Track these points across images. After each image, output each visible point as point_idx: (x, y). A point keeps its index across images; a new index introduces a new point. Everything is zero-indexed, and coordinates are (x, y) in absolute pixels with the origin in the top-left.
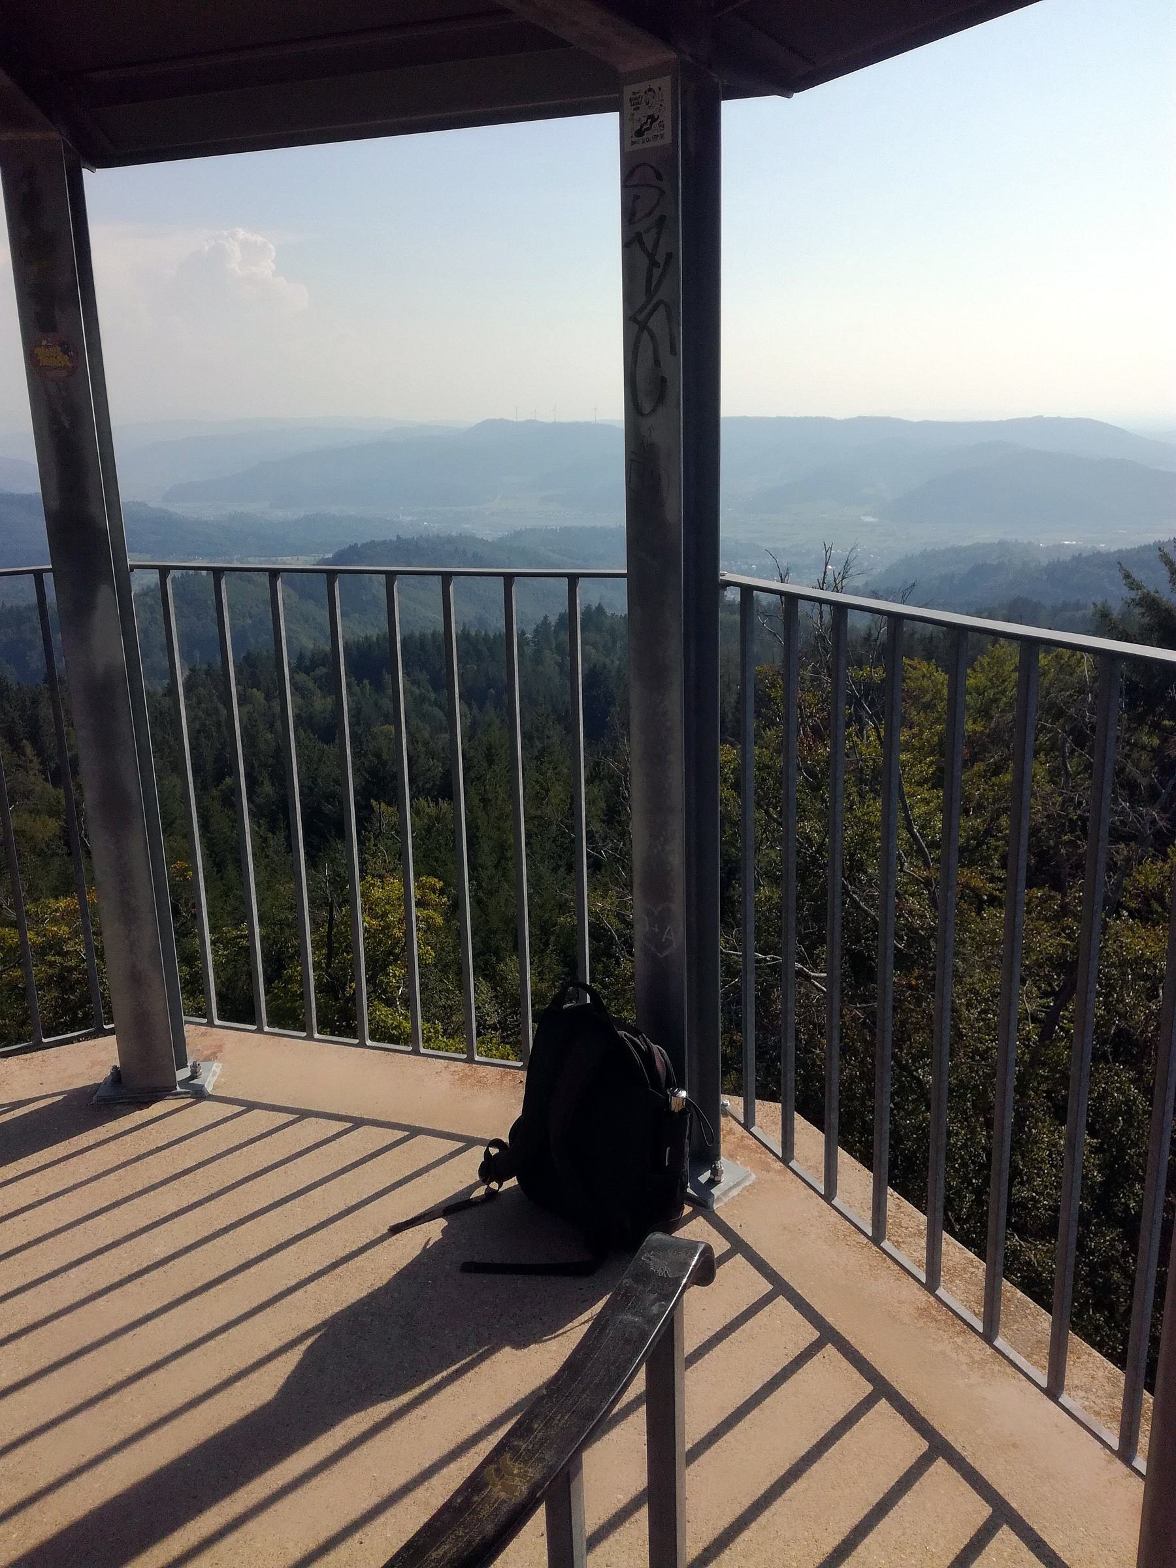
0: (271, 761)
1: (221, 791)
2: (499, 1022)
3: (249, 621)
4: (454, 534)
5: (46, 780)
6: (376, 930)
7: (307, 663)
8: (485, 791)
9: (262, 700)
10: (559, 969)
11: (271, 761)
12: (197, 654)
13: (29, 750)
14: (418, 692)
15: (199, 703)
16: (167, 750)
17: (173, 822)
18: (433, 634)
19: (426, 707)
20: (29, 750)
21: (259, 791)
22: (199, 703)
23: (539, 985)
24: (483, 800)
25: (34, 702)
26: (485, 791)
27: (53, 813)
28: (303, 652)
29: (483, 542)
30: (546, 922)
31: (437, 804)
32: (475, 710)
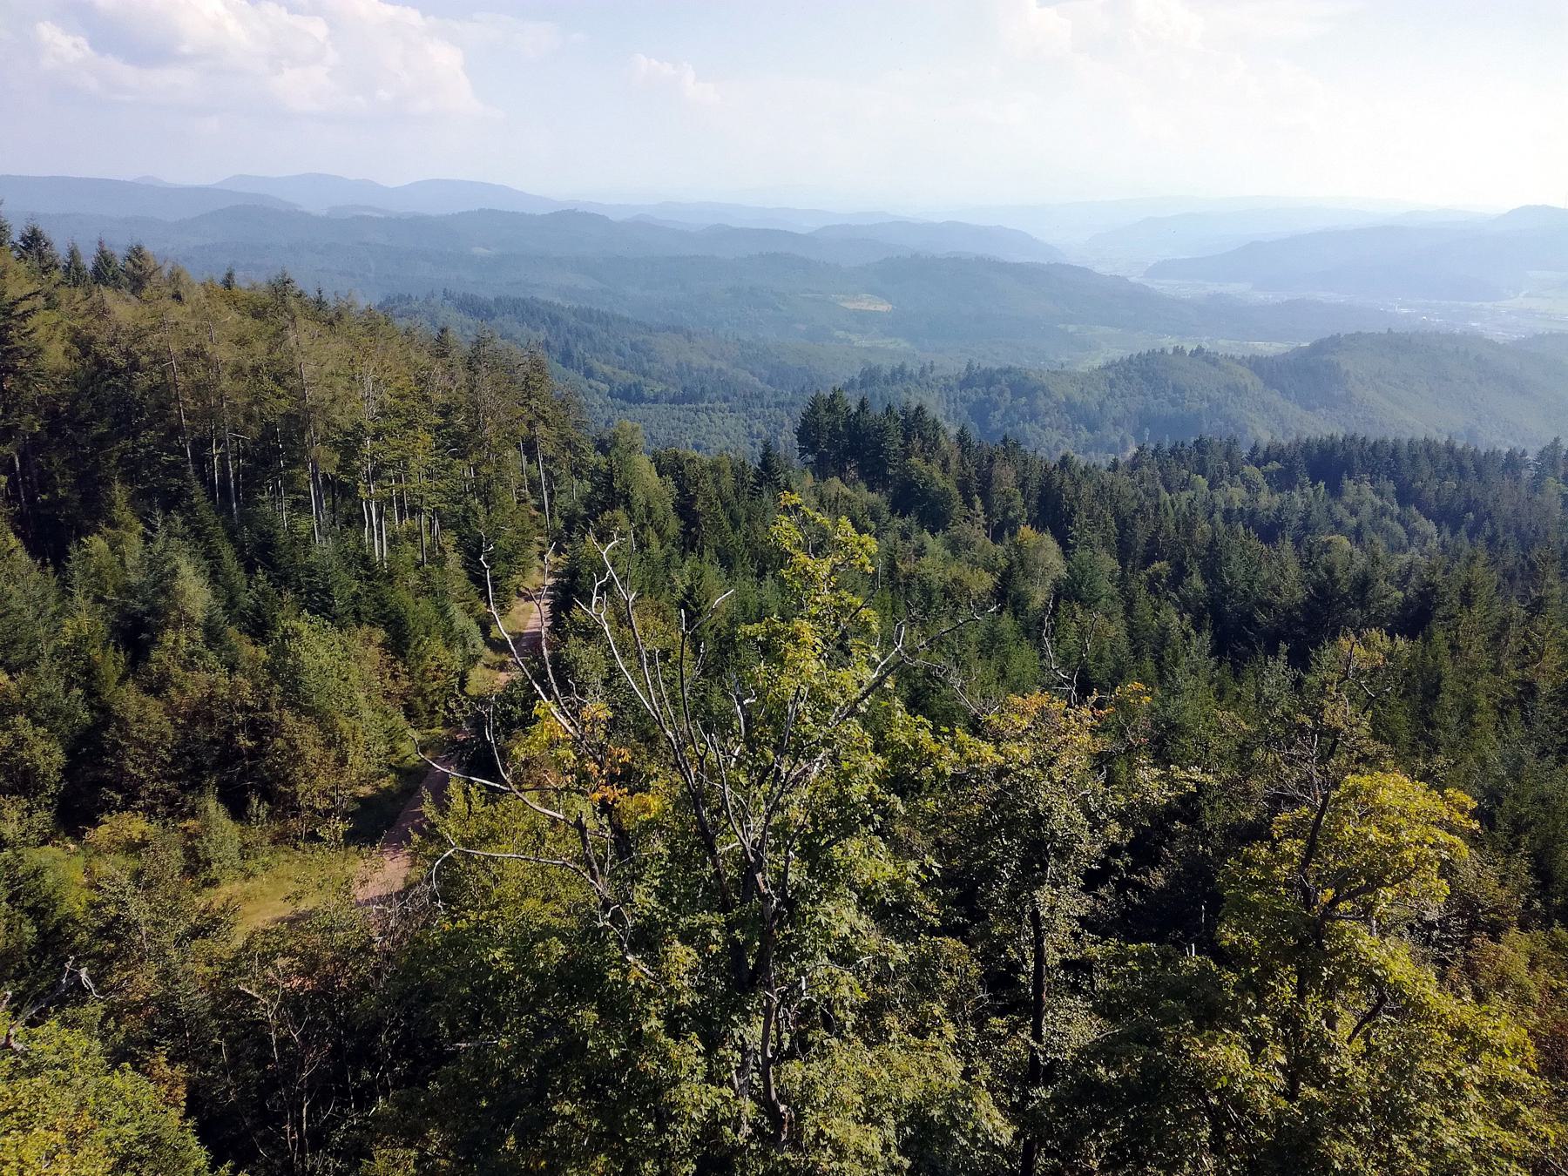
0: (1204, 553)
1: (1148, 575)
2: (1440, 921)
3: (1206, 405)
4: (1457, 331)
5: (987, 535)
6: (1383, 847)
7: (1260, 455)
8: (1457, 636)
9: (1205, 488)
10: (1530, 880)
11: (1204, 553)
12: (1147, 432)
13: (978, 505)
14: (1380, 503)
15: (1142, 481)
16: (1102, 526)
17: (1098, 600)
18: (1410, 442)
19: (1386, 521)
20: (978, 505)
21: (1186, 581)
22: (1142, 481)
23: (1499, 890)
24: (1451, 647)
25: (991, 460)
26: (1457, 636)
27: (990, 569)
28: (106, 248)
29: (1491, 344)
30: (1521, 817)
31: (1393, 639)
32: (1446, 534)
